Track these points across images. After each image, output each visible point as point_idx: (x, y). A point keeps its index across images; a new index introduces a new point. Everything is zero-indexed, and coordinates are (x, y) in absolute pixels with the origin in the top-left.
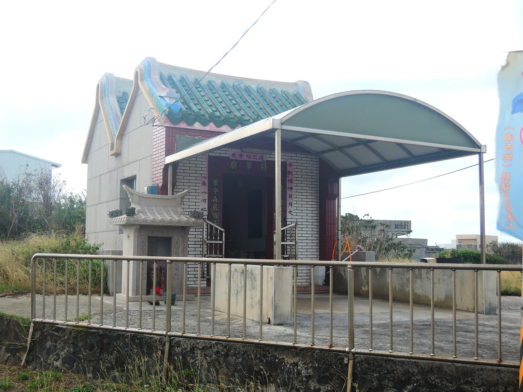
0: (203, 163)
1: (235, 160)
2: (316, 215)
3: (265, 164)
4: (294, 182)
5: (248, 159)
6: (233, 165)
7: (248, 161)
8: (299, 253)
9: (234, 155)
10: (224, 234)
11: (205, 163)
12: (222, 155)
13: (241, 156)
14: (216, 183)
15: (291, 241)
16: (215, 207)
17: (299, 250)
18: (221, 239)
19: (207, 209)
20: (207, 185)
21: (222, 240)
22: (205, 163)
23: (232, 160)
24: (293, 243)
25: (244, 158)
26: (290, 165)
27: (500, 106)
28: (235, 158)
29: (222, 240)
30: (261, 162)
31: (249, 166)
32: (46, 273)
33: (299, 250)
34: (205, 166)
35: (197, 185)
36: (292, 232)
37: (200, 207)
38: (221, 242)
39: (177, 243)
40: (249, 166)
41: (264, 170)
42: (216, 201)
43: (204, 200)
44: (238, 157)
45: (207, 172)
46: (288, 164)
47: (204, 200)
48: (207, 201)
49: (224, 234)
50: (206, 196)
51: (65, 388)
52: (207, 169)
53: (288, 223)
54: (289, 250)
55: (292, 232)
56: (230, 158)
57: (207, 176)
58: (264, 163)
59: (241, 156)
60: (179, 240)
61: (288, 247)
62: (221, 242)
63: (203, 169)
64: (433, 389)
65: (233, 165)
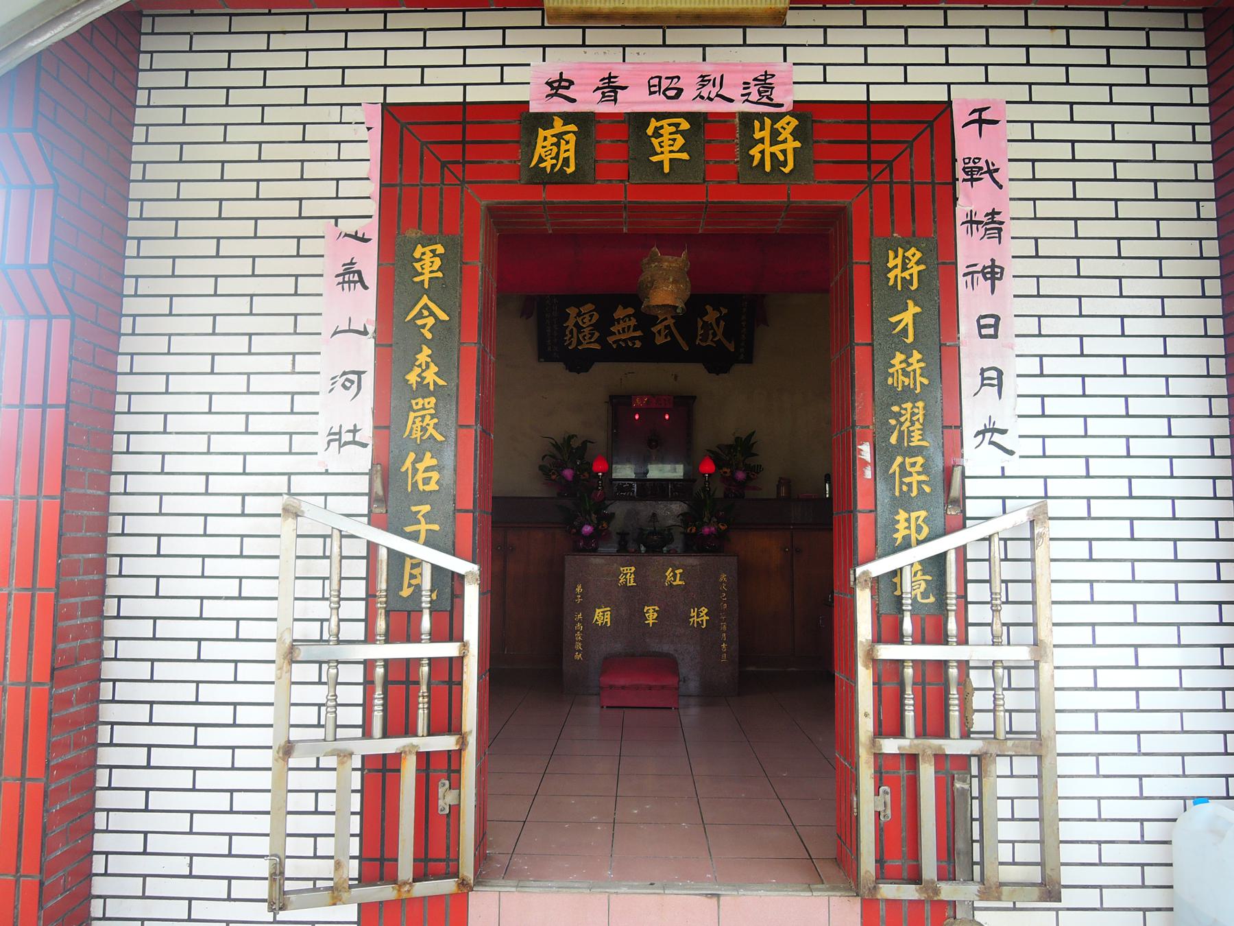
1: (568, 118)
2: (1201, 407)
3: (788, 125)
4: (1011, 229)
5: (660, 104)
6: (553, 150)
7: (660, 116)
8: (1062, 722)
16: (422, 419)
17: (1062, 700)
18: (448, 629)
19: (366, 434)
23: (545, 120)
24: (1021, 654)
25: (634, 100)
28: (568, 107)
30: (760, 116)
31: (668, 148)
32: (558, 122)
33: (1062, 700)
34: (362, 169)
36: (1008, 570)
37: (322, 425)
38: (449, 650)
40: (668, 148)
42: (431, 376)
43: (352, 379)
44: (588, 101)
45: (372, 207)
46: (960, 115)
47: (352, 379)
48: (368, 381)
50: (364, 353)
51: (815, 162)
53: (972, 508)
54: (980, 700)
55: (1008, 570)
57: (371, 228)
59: (610, 87)
61: (977, 678)
62: (449, 650)
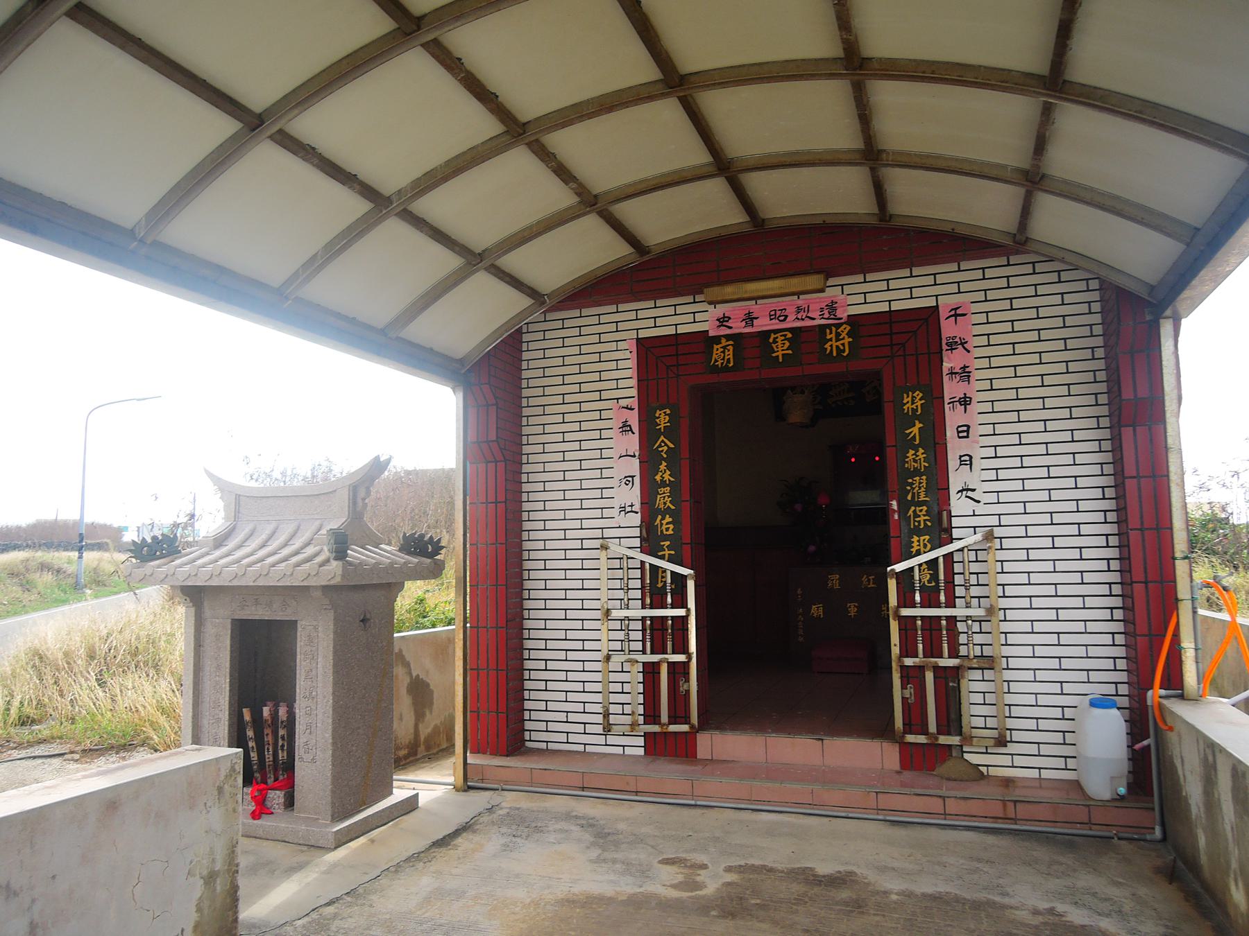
0: (621, 364)
1: (728, 337)
4: (976, 375)
6: (722, 355)
9: (723, 321)
10: (691, 585)
11: (628, 364)
12: (681, 330)
13: (750, 319)
14: (663, 419)
15: (968, 606)
16: (664, 499)
18: (680, 602)
19: (637, 507)
20: (636, 429)
21: (683, 604)
22: (628, 364)
23: (717, 339)
25: (763, 324)
26: (956, 314)
27: (847, 736)
28: (728, 332)
29: (683, 604)
31: (781, 348)
35: (605, 434)
37: (616, 503)
38: (681, 612)
39: (310, 640)
40: (781, 348)
41: (915, 411)
42: (667, 477)
43: (629, 479)
44: (738, 327)
45: (634, 392)
46: (943, 313)
47: (629, 479)
48: (637, 480)
49: (691, 585)
50: (634, 467)
52: (633, 382)
56: (711, 334)
57: (634, 403)
58: (838, 326)
59: (750, 319)
60: (316, 628)
62: (681, 612)
63: (622, 384)
64: (849, 334)
65: (722, 355)
